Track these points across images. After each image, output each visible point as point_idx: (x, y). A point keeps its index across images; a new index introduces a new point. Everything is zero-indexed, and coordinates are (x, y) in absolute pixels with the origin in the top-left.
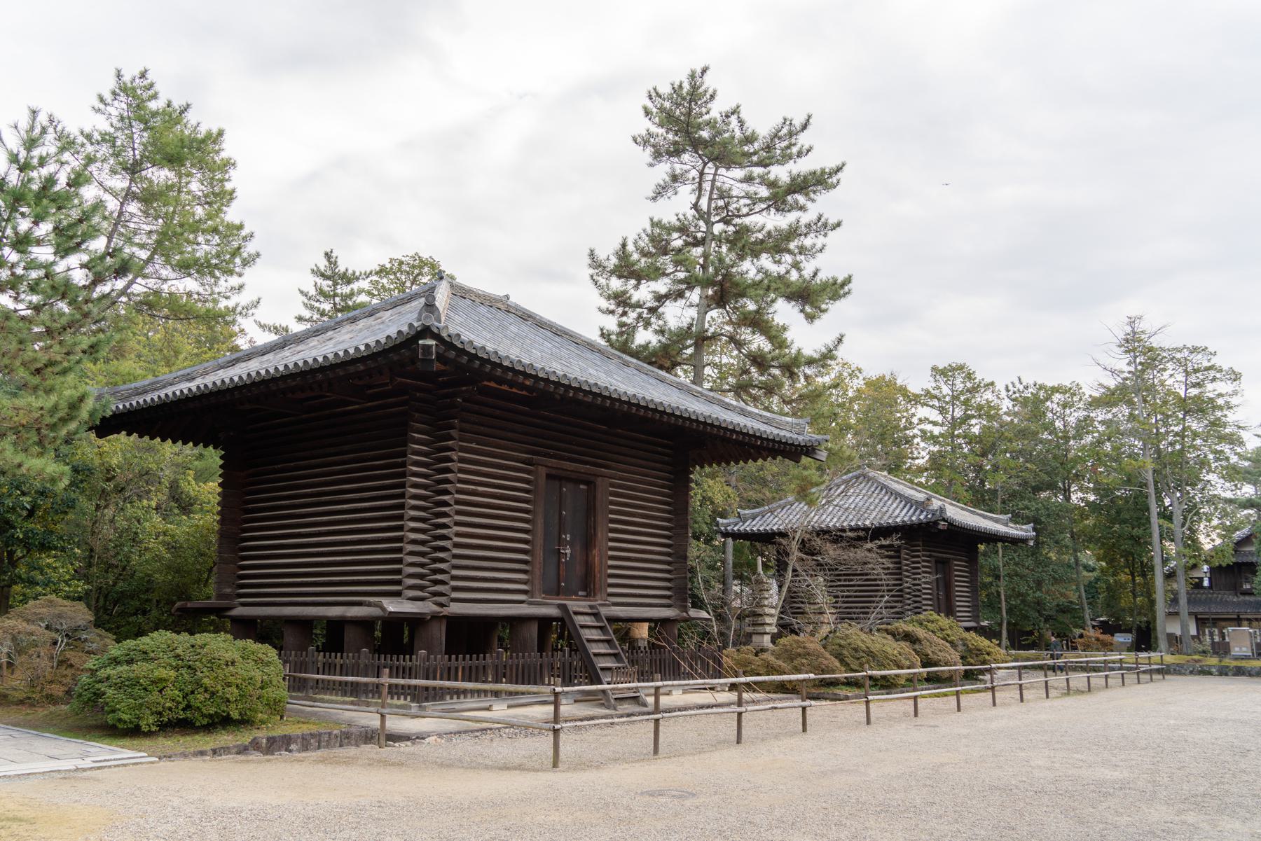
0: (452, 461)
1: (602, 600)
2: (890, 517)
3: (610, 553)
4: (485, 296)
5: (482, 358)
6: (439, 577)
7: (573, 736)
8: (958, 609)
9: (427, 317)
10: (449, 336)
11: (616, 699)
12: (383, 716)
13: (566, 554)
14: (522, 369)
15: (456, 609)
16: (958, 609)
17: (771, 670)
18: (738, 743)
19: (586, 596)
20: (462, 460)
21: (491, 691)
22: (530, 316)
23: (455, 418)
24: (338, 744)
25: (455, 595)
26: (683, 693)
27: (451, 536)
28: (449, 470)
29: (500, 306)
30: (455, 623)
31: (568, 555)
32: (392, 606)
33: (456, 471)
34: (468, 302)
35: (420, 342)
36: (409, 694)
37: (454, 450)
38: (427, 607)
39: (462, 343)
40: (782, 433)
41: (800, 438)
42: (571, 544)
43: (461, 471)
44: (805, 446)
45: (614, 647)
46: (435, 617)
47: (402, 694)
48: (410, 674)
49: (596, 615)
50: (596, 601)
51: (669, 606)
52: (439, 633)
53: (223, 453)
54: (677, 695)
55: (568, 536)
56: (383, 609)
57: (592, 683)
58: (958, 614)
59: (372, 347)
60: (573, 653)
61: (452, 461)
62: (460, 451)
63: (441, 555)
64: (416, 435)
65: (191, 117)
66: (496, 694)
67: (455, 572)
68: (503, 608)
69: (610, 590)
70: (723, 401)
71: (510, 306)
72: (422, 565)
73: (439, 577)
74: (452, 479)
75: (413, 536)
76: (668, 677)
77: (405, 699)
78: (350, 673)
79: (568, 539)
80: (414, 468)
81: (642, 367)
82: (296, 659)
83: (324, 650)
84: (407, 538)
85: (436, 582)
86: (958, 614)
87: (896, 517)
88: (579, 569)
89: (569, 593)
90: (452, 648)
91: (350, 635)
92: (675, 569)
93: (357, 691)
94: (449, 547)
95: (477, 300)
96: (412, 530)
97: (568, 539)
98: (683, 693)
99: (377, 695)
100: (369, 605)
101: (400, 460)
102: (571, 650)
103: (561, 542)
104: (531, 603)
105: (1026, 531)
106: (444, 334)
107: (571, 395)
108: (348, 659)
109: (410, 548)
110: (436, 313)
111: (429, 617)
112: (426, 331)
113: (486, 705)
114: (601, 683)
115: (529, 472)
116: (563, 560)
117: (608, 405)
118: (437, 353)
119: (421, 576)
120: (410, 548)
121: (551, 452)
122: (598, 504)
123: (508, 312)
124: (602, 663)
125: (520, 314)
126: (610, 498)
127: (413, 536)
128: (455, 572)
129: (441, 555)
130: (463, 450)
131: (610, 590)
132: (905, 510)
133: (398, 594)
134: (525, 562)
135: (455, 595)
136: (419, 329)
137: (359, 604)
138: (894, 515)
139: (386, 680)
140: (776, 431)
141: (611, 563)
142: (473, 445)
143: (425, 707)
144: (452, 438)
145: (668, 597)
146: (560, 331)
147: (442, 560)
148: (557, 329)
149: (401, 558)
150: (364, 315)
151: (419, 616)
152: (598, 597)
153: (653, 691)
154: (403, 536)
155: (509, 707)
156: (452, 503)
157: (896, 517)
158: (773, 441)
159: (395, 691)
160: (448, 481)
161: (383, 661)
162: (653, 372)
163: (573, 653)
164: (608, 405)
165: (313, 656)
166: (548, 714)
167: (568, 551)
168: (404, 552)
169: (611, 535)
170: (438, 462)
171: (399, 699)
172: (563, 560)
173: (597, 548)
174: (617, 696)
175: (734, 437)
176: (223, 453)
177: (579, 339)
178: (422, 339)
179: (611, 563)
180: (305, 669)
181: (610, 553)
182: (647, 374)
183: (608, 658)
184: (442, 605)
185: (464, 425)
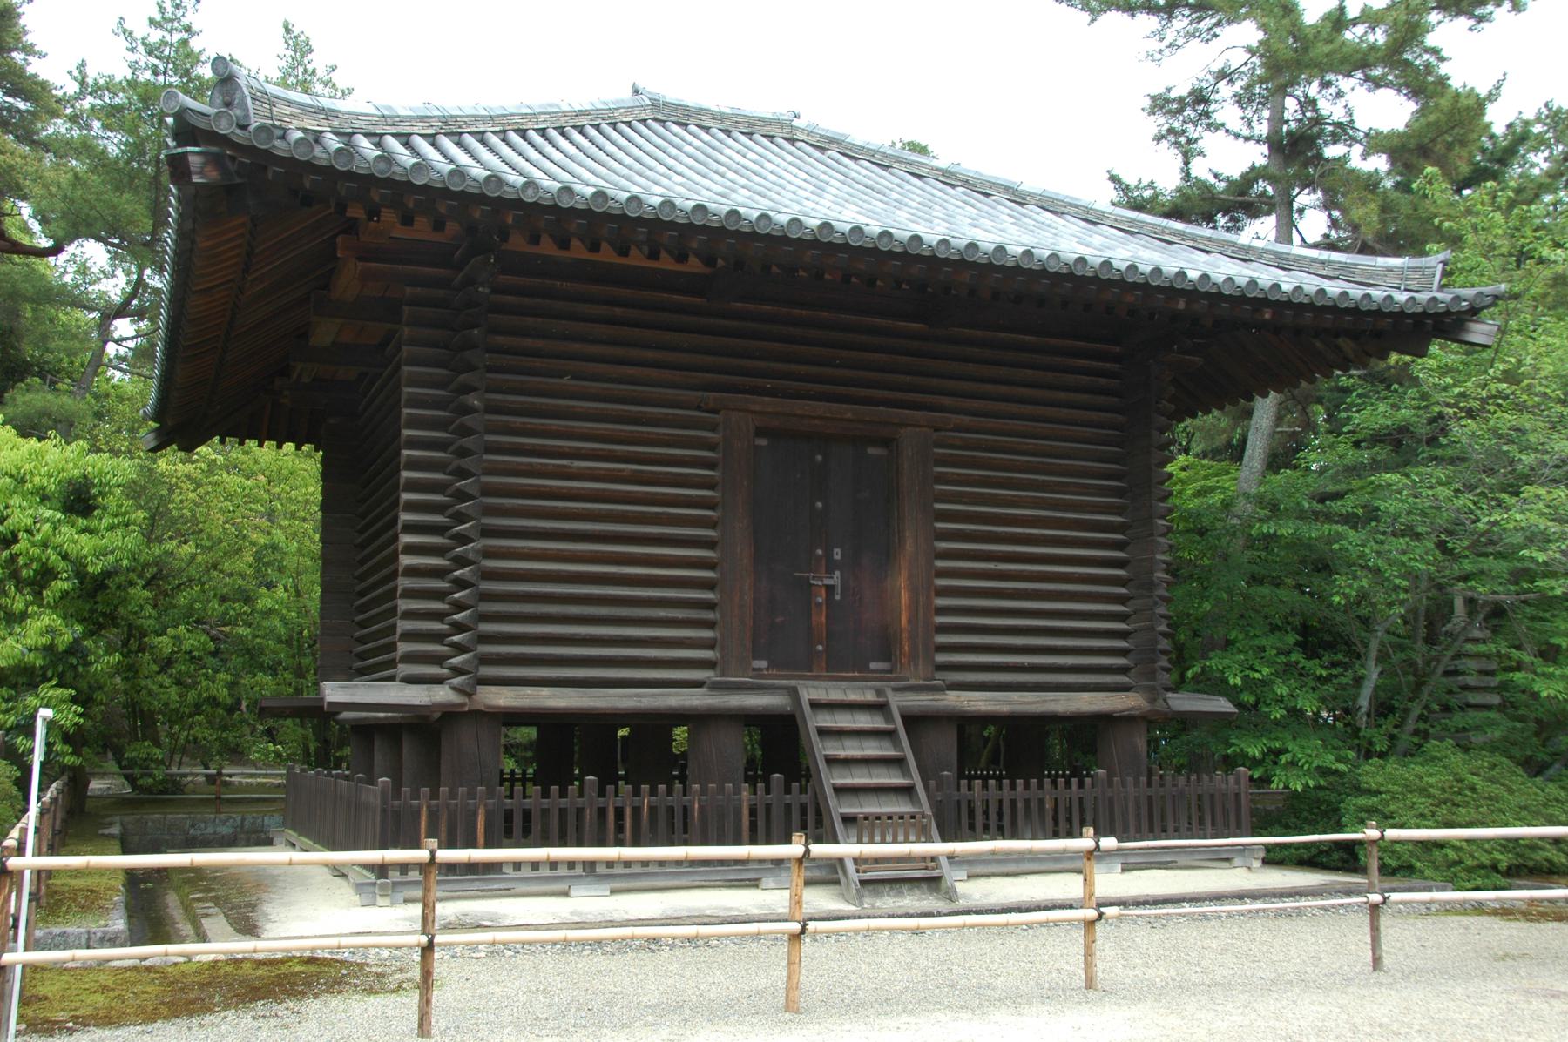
7: (1143, 938)
11: (863, 882)
18: (1375, 970)
22: (832, 140)
23: (473, 327)
26: (1123, 870)
48: (620, 828)
51: (1125, 688)
60: (964, 782)
62: (487, 391)
65: (1257, 165)
67: (486, 627)
68: (638, 696)
69: (941, 658)
70: (1234, 244)
82: (1040, 794)
98: (1123, 870)
104: (716, 687)
128: (486, 627)
131: (941, 658)
134: (710, 606)
141: (941, 602)
145: (1123, 670)
155: (613, 892)
166: (411, 919)
179: (941, 602)
183: (893, 797)
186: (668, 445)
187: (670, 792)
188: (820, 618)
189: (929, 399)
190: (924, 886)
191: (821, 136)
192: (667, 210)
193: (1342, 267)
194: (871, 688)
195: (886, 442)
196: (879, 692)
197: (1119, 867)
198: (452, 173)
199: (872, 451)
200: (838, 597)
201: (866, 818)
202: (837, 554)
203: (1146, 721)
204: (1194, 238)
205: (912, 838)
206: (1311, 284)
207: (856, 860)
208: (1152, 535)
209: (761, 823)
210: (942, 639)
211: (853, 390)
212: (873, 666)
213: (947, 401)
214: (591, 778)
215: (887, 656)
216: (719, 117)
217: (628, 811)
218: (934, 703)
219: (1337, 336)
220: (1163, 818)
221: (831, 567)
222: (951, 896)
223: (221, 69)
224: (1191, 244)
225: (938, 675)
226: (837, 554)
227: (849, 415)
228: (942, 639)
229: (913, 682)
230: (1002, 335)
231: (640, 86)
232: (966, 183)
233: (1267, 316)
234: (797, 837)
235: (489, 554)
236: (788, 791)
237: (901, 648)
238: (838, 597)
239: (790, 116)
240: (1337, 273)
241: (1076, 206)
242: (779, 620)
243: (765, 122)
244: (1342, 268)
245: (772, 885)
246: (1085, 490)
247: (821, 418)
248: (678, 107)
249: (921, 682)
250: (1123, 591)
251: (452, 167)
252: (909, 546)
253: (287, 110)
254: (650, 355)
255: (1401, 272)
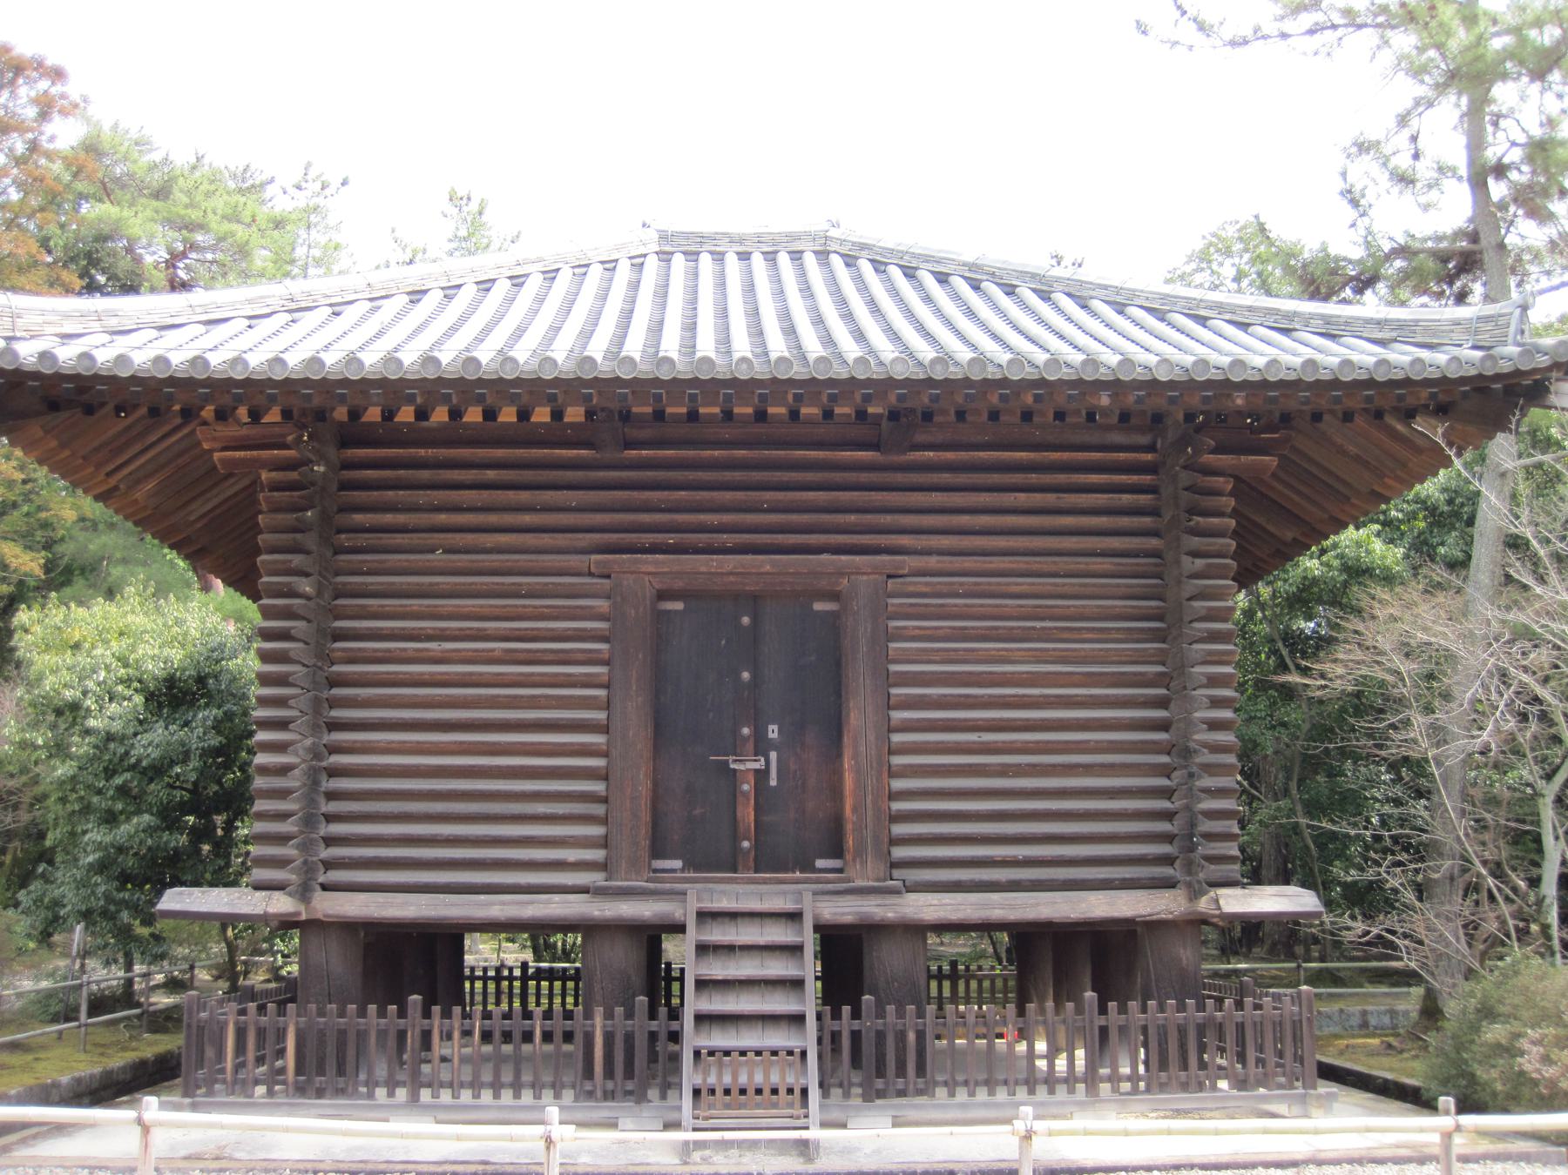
51: (1169, 884)
145: (1168, 860)
186: (556, 618)
187: (1162, 1008)
188: (747, 814)
191: (854, 244)
192: (1089, 369)
195: (835, 596)
197: (890, 1120)
198: (1085, 363)
199: (818, 606)
200: (773, 783)
201: (711, 1053)
202: (773, 732)
203: (286, 924)
205: (676, 1080)
208: (1185, 688)
211: (780, 538)
212: (820, 863)
214: (642, 998)
215: (837, 851)
217: (911, 1036)
218: (860, 903)
219: (1409, 415)
220: (1261, 1049)
221: (761, 746)
224: (1227, 317)
225: (896, 873)
226: (773, 732)
227: (768, 568)
229: (860, 883)
230: (981, 454)
233: (1239, 402)
236: (1103, 1010)
238: (773, 783)
239: (826, 226)
240: (1394, 334)
241: (1106, 287)
242: (697, 812)
245: (631, 1126)
249: (876, 884)
250: (1165, 759)
251: (1047, 356)
253: (40, 319)
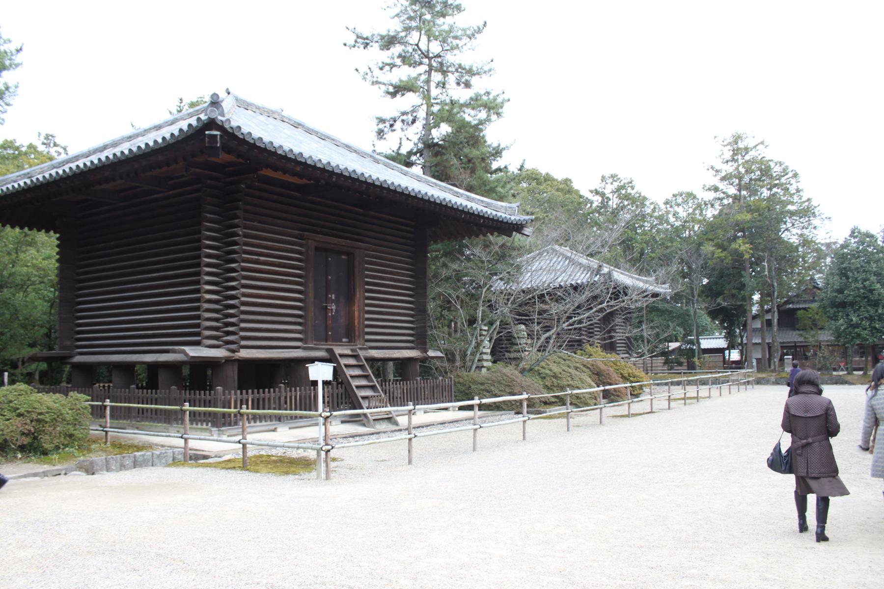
0: (238, 235)
1: (360, 345)
2: (573, 280)
3: (367, 308)
4: (264, 108)
5: (259, 147)
6: (230, 329)
8: (618, 345)
9: (212, 111)
10: (232, 128)
11: (374, 420)
12: (186, 440)
13: (332, 309)
14: (294, 158)
15: (244, 354)
16: (618, 345)
17: (661, 378)
19: (349, 342)
20: (246, 236)
21: (275, 416)
22: (299, 124)
23: (239, 201)
24: (151, 464)
25: (243, 343)
27: (239, 296)
28: (235, 243)
29: (276, 116)
30: (245, 364)
31: (334, 311)
32: (193, 352)
33: (242, 244)
34: (250, 112)
35: (207, 132)
36: (209, 421)
37: (239, 227)
38: (220, 353)
39: (242, 134)
40: (499, 214)
41: (513, 218)
42: (337, 302)
43: (246, 244)
44: (516, 224)
45: (371, 380)
46: (228, 361)
47: (204, 421)
49: (356, 357)
50: (356, 345)
52: (233, 373)
53: (59, 242)
54: (424, 414)
55: (333, 295)
56: (186, 354)
57: (355, 408)
58: (618, 349)
59: (168, 139)
61: (238, 235)
62: (244, 228)
63: (232, 311)
64: (208, 215)
66: (279, 418)
67: (243, 325)
68: (283, 352)
69: (367, 337)
71: (284, 117)
72: (217, 320)
73: (230, 329)
74: (238, 251)
75: (208, 296)
76: (396, 404)
77: (207, 425)
78: (227, 406)
79: (333, 298)
80: (208, 242)
81: (389, 163)
83: (147, 388)
84: (204, 298)
85: (228, 333)
86: (618, 349)
87: (578, 279)
88: (343, 321)
89: (337, 340)
90: (243, 385)
91: (162, 377)
92: (417, 320)
93: (169, 419)
94: (238, 305)
95: (257, 111)
96: (208, 292)
97: (333, 298)
99: (194, 422)
100: (174, 352)
101: (196, 236)
102: (338, 384)
103: (327, 300)
104: (305, 349)
105: (666, 289)
106: (227, 126)
107: (334, 179)
108: (161, 393)
109: (206, 306)
110: (220, 109)
111: (223, 361)
112: (211, 124)
113: (273, 428)
114: (362, 408)
115: (301, 245)
116: (330, 314)
117: (364, 189)
118: (222, 142)
119: (216, 329)
120: (206, 306)
121: (319, 230)
122: (357, 270)
123: (283, 121)
124: (361, 393)
125: (292, 123)
126: (366, 266)
127: (208, 296)
128: (243, 325)
129: (232, 311)
130: (246, 227)
131: (367, 337)
132: (583, 275)
133: (197, 343)
135: (243, 343)
136: (205, 122)
137: (167, 351)
138: (576, 278)
139: (476, 401)
140: (494, 213)
141: (367, 316)
142: (255, 224)
143: (223, 431)
144: (238, 218)
146: (324, 135)
147: (232, 316)
148: (321, 134)
149: (200, 314)
150: (167, 124)
151: (212, 360)
152: (358, 342)
153: (407, 412)
154: (200, 297)
156: (239, 270)
157: (578, 279)
158: (493, 219)
159: (195, 417)
160: (234, 252)
161: (198, 396)
162: (398, 167)
163: (340, 386)
164: (364, 189)
165: (134, 393)
167: (334, 307)
168: (202, 310)
169: (367, 294)
170: (226, 238)
171: (197, 424)
172: (330, 314)
173: (356, 305)
174: (374, 418)
175: (463, 216)
176: (59, 242)
177: (339, 141)
178: (207, 131)
179: (367, 316)
180: (214, 404)
181: (367, 308)
182: (393, 169)
184: (233, 351)
185: (247, 207)
189: (361, 238)
190: (386, 421)
193: (488, 204)
194: (349, 349)
196: (352, 350)
204: (440, 186)
206: (480, 208)
207: (371, 413)
209: (261, 403)
210: (367, 330)
213: (368, 240)
214: (173, 387)
216: (258, 108)
222: (396, 424)
223: (215, 98)
227: (344, 244)
228: (367, 330)
231: (230, 90)
232: (355, 151)
234: (476, 398)
235: (245, 295)
237: (355, 333)
243: (273, 112)
244: (487, 204)
246: (403, 275)
247: (336, 244)
248: (244, 102)
250: (412, 312)
252: (358, 295)
254: (284, 215)
255: (506, 208)
